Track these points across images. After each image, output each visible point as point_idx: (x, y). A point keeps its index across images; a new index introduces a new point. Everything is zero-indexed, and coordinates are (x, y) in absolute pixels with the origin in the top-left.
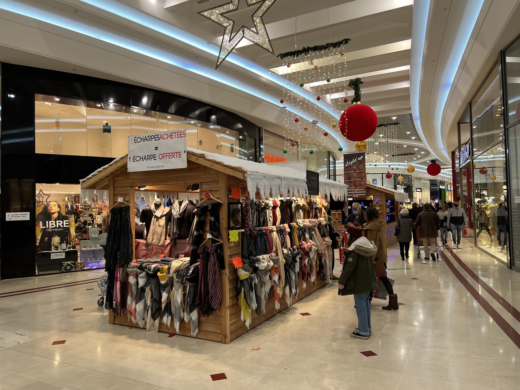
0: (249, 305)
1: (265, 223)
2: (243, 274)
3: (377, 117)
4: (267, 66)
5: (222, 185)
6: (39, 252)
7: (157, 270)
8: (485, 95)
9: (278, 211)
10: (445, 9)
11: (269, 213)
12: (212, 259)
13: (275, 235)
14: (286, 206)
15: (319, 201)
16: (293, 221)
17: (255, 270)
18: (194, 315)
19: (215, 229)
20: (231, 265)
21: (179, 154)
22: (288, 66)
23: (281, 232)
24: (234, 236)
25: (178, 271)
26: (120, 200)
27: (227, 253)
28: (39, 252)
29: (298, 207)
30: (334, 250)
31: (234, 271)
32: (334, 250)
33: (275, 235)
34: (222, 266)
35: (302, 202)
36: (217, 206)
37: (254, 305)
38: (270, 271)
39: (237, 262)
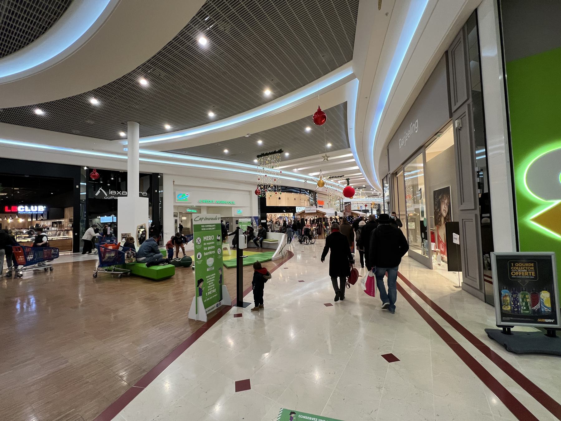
0: (326, 234)
1: (328, 221)
2: (325, 229)
3: (511, 330)
4: (307, 174)
5: (322, 215)
6: (174, 241)
7: (310, 229)
8: (375, 176)
9: (330, 219)
10: (367, 98)
11: (328, 219)
12: (321, 226)
13: (329, 223)
14: (331, 218)
15: (337, 217)
16: (92, 237)
17: (327, 229)
18: (318, 235)
19: (321, 222)
20: (324, 227)
21: (315, 210)
22: (462, 283)
23: (330, 223)
24: (324, 223)
25: (315, 228)
26: (303, 217)
27: (323, 225)
28: (174, 241)
29: (333, 218)
30: (488, 192)
31: (324, 228)
32: (488, 192)
33: (329, 223)
34: (322, 227)
35: (333, 217)
36: (321, 218)
37: (327, 234)
38: (329, 229)
39: (324, 227)
